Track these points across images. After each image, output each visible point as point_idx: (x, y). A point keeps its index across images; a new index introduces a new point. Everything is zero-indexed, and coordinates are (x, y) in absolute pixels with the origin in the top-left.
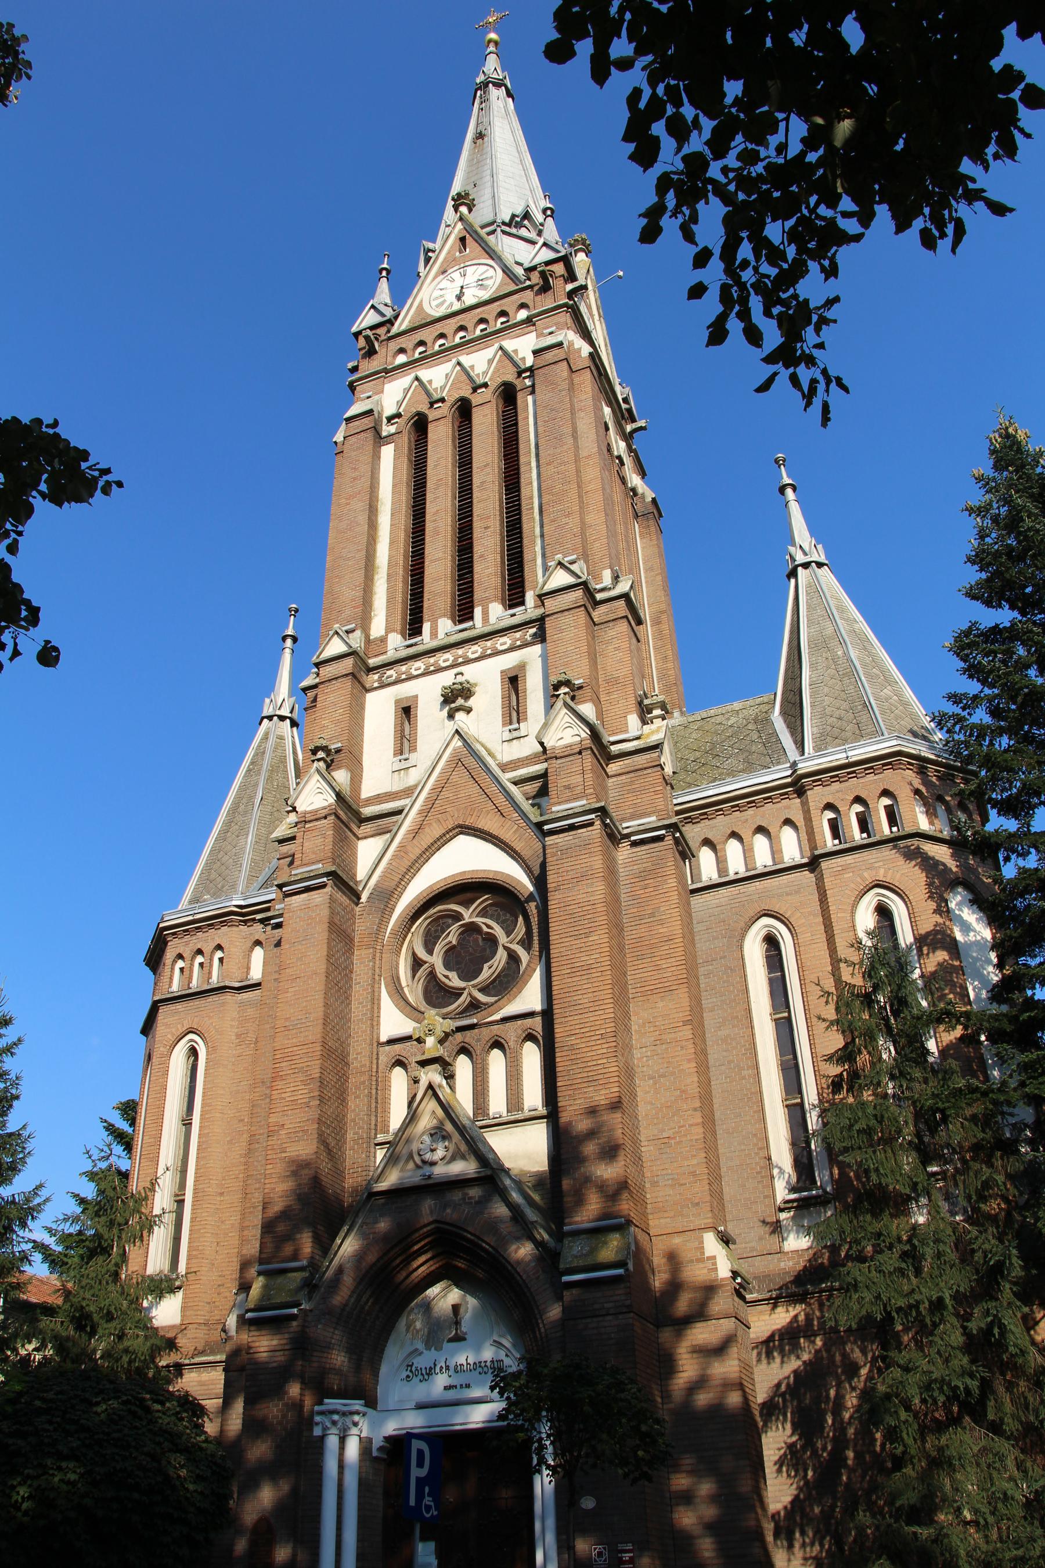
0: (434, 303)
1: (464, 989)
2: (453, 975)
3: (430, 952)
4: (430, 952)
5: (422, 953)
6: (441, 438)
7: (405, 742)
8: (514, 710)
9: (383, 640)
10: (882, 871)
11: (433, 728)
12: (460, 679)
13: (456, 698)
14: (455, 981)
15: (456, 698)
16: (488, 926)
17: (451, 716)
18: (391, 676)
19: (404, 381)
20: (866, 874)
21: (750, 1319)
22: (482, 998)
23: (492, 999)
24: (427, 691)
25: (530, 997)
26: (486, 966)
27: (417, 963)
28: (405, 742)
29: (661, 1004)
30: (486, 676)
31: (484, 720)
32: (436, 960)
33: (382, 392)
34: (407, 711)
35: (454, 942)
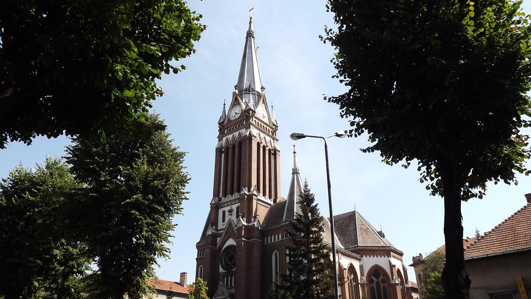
6: (230, 152)
28: (224, 220)
32: (227, 259)
34: (224, 213)
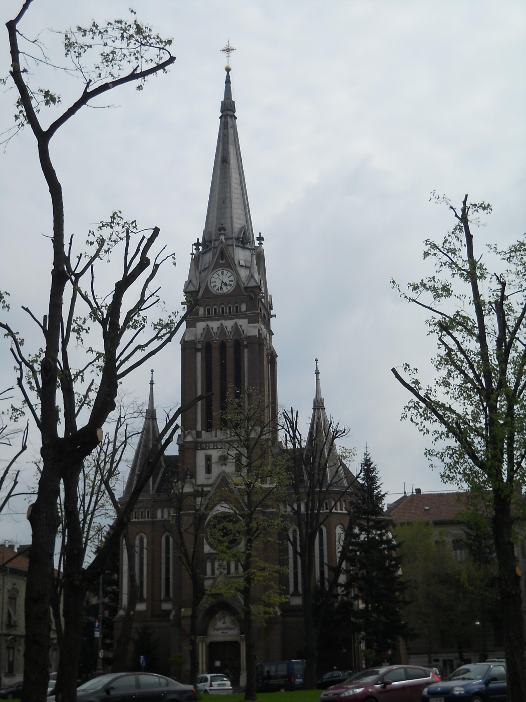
7: (208, 470)
11: (216, 470)
13: (223, 459)
24: (215, 454)
31: (230, 468)
34: (208, 458)
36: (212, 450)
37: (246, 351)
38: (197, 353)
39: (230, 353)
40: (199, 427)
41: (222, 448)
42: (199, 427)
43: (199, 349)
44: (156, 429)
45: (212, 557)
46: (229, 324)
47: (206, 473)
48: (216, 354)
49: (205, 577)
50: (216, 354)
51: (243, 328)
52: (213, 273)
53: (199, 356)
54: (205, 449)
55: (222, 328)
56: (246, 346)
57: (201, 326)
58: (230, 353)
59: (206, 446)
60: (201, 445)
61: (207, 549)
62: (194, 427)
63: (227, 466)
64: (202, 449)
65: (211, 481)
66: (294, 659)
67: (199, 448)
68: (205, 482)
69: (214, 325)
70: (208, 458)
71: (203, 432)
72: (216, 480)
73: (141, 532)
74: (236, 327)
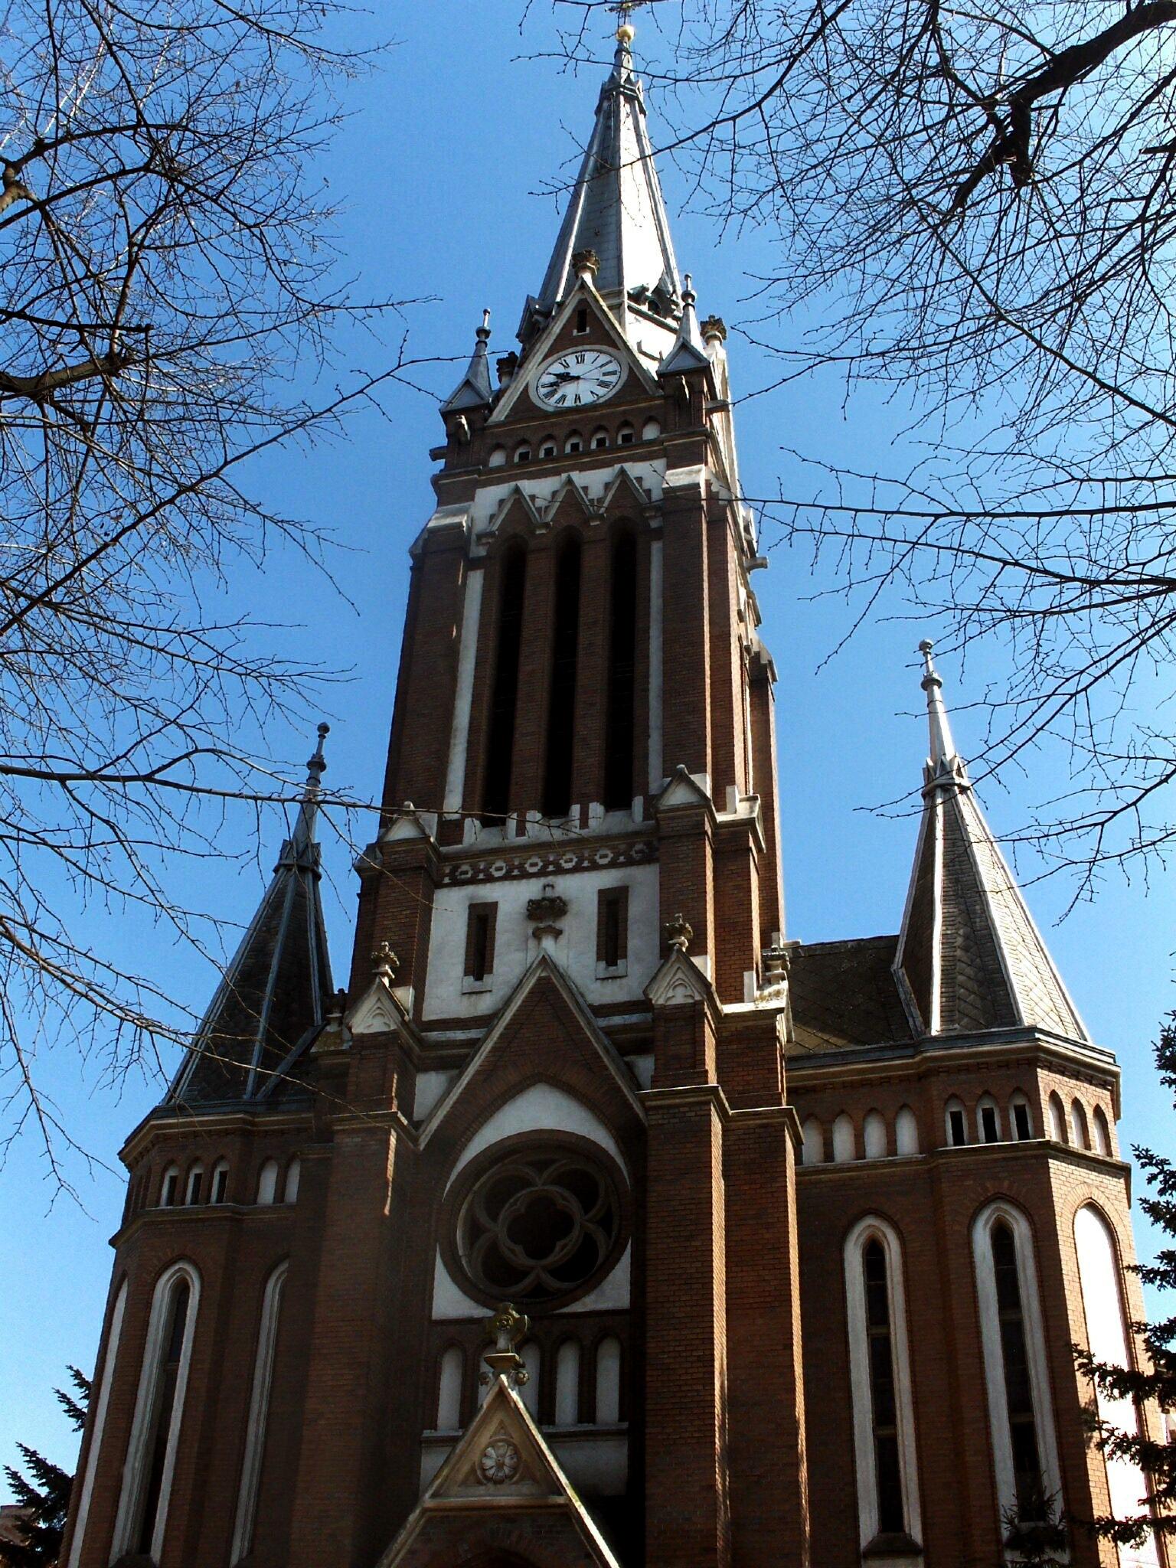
0: (543, 391)
1: (532, 1268)
2: (519, 1249)
3: (494, 1217)
4: (494, 1217)
5: (483, 1219)
7: (479, 958)
8: (611, 945)
9: (458, 825)
10: (1006, 1183)
11: (511, 959)
12: (549, 893)
13: (546, 914)
14: (518, 1256)
15: (546, 914)
16: (565, 1199)
17: (537, 935)
18: (466, 873)
19: (500, 491)
20: (988, 1185)
21: (1096, 132)
22: (553, 1283)
23: (566, 1285)
24: (512, 898)
25: (615, 1291)
26: (559, 1244)
27: (475, 1231)
29: (760, 1321)
30: (582, 890)
31: (574, 952)
32: (499, 1230)
33: (473, 499)
34: (482, 920)
35: (523, 1210)
36: (497, 886)
37: (656, 547)
38: (471, 574)
39: (596, 565)
40: (453, 802)
41: (542, 873)
42: (453, 802)
43: (480, 559)
44: (311, 904)
45: (470, 1341)
46: (594, 481)
47: (467, 973)
48: (541, 574)
49: (427, 1433)
50: (541, 574)
51: (646, 485)
52: (550, 360)
53: (475, 582)
54: (473, 881)
55: (572, 497)
56: (658, 534)
57: (488, 500)
58: (596, 565)
59: (477, 871)
60: (455, 868)
61: (448, 1300)
62: (432, 799)
63: (563, 939)
64: (457, 883)
65: (485, 1005)
66: (927, 1023)
67: (447, 880)
68: (463, 1009)
69: (540, 489)
70: (482, 920)
71: (468, 821)
72: (508, 1002)
73: (180, 1258)
74: (624, 485)
